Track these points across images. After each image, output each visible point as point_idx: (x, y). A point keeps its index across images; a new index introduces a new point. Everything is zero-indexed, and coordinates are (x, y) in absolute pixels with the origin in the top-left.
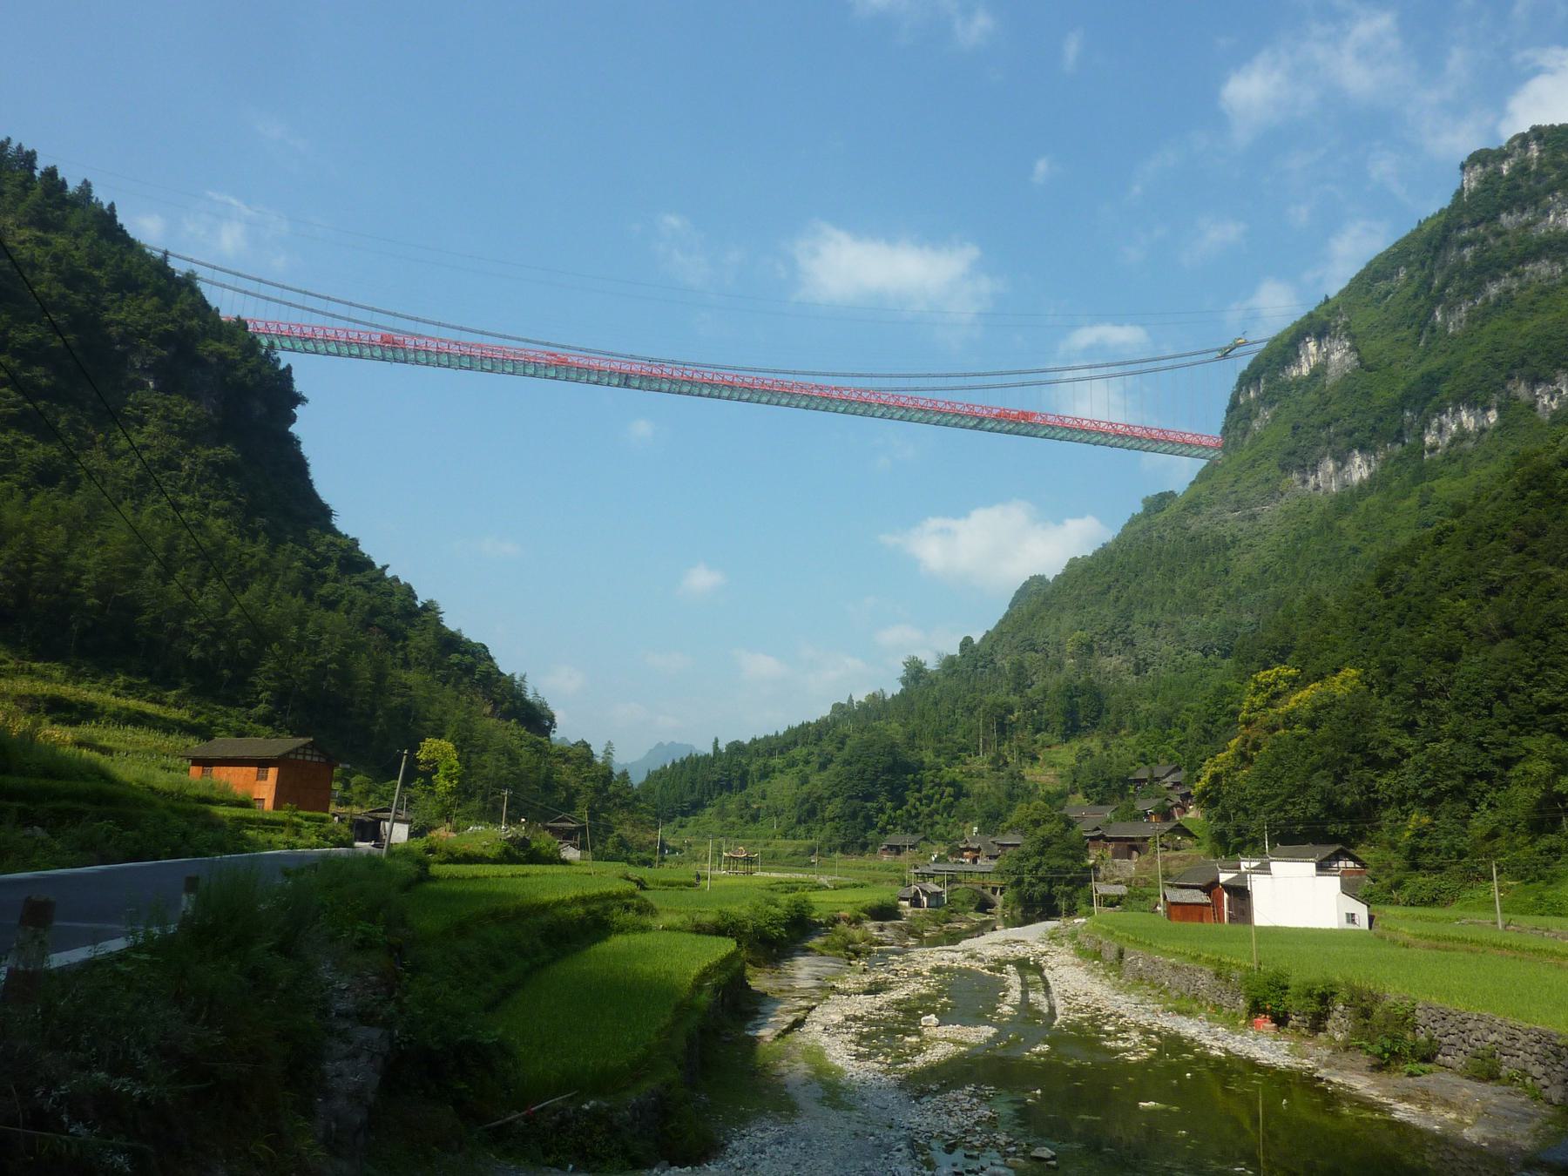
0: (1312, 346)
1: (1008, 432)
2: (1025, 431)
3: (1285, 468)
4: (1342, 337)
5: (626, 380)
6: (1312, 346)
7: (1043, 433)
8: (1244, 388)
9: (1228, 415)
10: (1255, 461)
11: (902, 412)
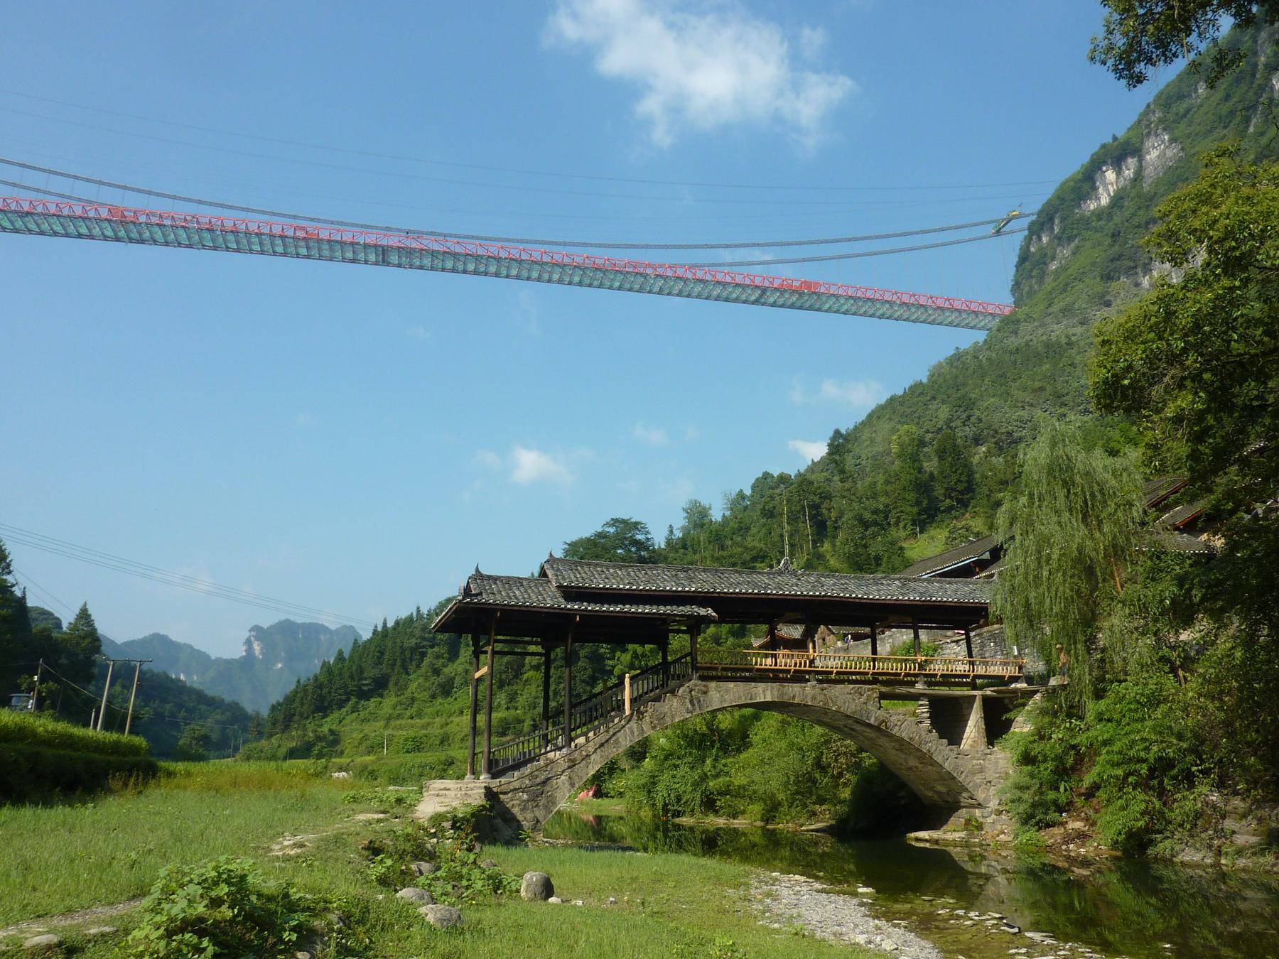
0: (1110, 175)
1: (792, 306)
2: (808, 304)
3: (1108, 277)
4: (1159, 131)
5: (383, 255)
6: (1110, 175)
7: (827, 306)
8: (1034, 237)
9: (1017, 271)
10: (1067, 285)
11: (680, 285)
